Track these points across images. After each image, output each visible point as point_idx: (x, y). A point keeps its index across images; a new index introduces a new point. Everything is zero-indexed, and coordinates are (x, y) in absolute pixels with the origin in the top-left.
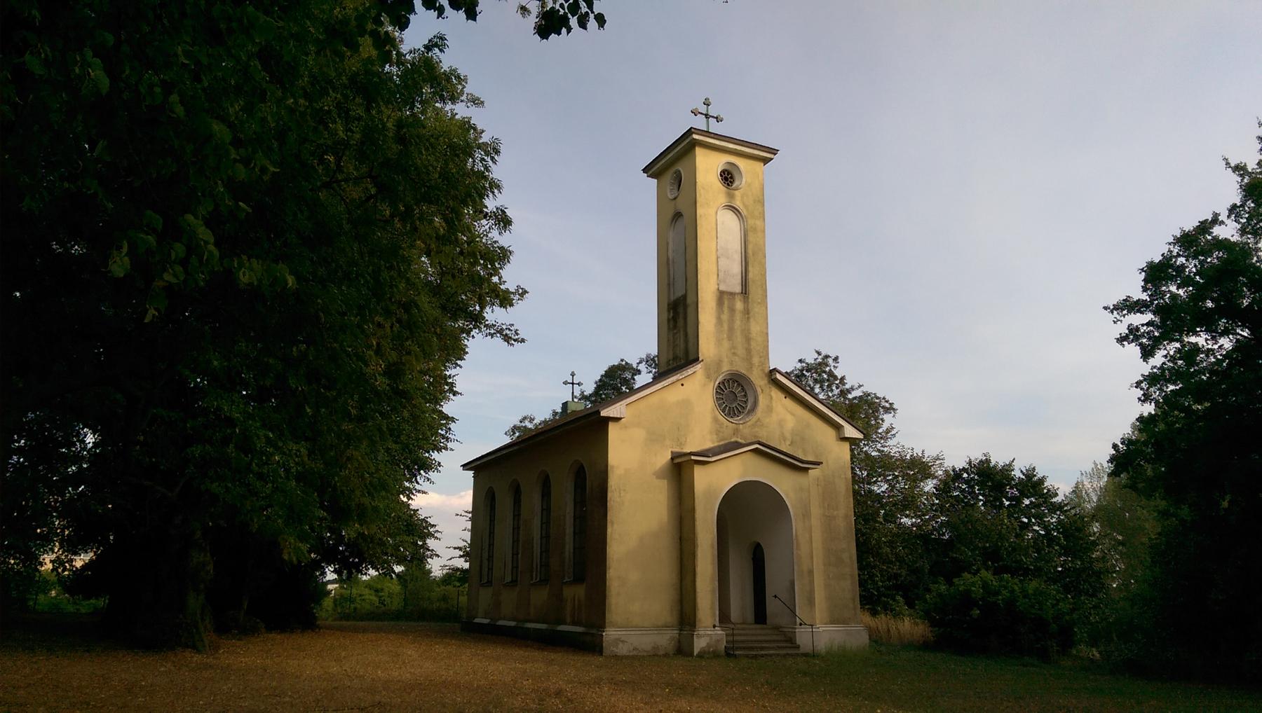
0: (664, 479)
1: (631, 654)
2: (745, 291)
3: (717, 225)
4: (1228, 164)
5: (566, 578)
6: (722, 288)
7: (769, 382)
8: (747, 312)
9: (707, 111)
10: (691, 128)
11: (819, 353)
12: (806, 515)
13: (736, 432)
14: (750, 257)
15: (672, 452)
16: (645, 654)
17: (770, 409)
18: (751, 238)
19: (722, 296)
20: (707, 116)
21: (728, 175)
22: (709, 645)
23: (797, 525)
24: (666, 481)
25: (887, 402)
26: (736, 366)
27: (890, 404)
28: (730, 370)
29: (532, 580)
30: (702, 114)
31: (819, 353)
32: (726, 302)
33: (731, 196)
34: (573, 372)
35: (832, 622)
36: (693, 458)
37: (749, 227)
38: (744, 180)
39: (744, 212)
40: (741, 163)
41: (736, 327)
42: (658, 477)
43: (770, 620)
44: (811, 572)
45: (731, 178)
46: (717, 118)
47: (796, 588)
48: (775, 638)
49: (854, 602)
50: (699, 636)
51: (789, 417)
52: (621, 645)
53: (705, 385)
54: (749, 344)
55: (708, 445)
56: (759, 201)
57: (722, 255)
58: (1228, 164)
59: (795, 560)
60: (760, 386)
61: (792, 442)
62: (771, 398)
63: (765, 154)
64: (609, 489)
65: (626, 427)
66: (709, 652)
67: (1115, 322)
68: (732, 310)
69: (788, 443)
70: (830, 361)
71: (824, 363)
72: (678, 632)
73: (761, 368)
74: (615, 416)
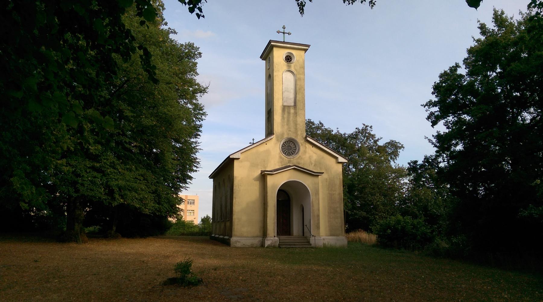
1: (242, 246)
2: (295, 105)
3: (283, 79)
4: (474, 39)
5: (227, 219)
6: (285, 104)
7: (305, 141)
8: (296, 113)
9: (284, 31)
10: (270, 40)
11: (364, 125)
12: (317, 193)
13: (289, 162)
14: (298, 90)
15: (261, 171)
16: (248, 246)
17: (305, 152)
18: (298, 83)
19: (284, 108)
20: (284, 33)
21: (289, 57)
23: (312, 197)
24: (258, 182)
25: (400, 144)
27: (402, 145)
28: (287, 137)
29: (222, 219)
30: (281, 32)
31: (364, 125)
32: (286, 110)
33: (289, 67)
34: (253, 139)
35: (331, 235)
36: (266, 172)
37: (297, 78)
38: (295, 59)
39: (295, 72)
40: (294, 52)
41: (290, 120)
42: (255, 181)
43: (305, 236)
44: (318, 216)
45: (291, 58)
46: (288, 33)
47: (311, 222)
48: (305, 241)
49: (342, 228)
50: (267, 240)
52: (238, 243)
53: (276, 144)
54: (296, 126)
55: (277, 167)
56: (302, 67)
57: (286, 91)
58: (474, 39)
59: (311, 211)
60: (301, 143)
61: (315, 165)
62: (306, 148)
63: (305, 48)
64: (234, 186)
65: (242, 162)
66: (272, 246)
67: (426, 111)
68: (289, 113)
69: (313, 165)
70: (369, 129)
71: (366, 129)
72: (262, 238)
74: (236, 158)
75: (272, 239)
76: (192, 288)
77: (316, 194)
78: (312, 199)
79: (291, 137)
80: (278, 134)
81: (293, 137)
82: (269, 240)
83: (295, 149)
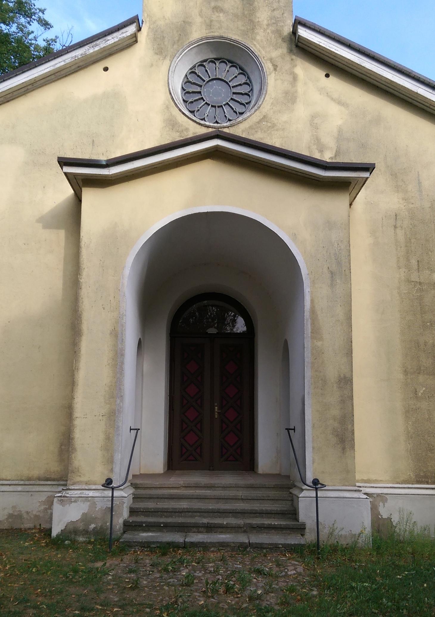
0: (58, 228)
7: (291, 51)
22: (86, 518)
26: (220, 28)
28: (207, 38)
42: (47, 226)
51: (334, 110)
60: (271, 60)
66: (86, 532)
73: (273, 28)
75: (91, 494)
76: (371, 538)
77: (332, 273)
78: (312, 301)
79: (225, 35)
80: (161, 23)
81: (234, 37)
82: (77, 499)
83: (245, 89)
